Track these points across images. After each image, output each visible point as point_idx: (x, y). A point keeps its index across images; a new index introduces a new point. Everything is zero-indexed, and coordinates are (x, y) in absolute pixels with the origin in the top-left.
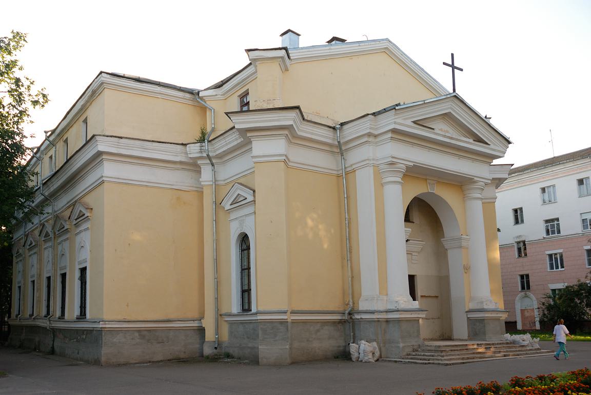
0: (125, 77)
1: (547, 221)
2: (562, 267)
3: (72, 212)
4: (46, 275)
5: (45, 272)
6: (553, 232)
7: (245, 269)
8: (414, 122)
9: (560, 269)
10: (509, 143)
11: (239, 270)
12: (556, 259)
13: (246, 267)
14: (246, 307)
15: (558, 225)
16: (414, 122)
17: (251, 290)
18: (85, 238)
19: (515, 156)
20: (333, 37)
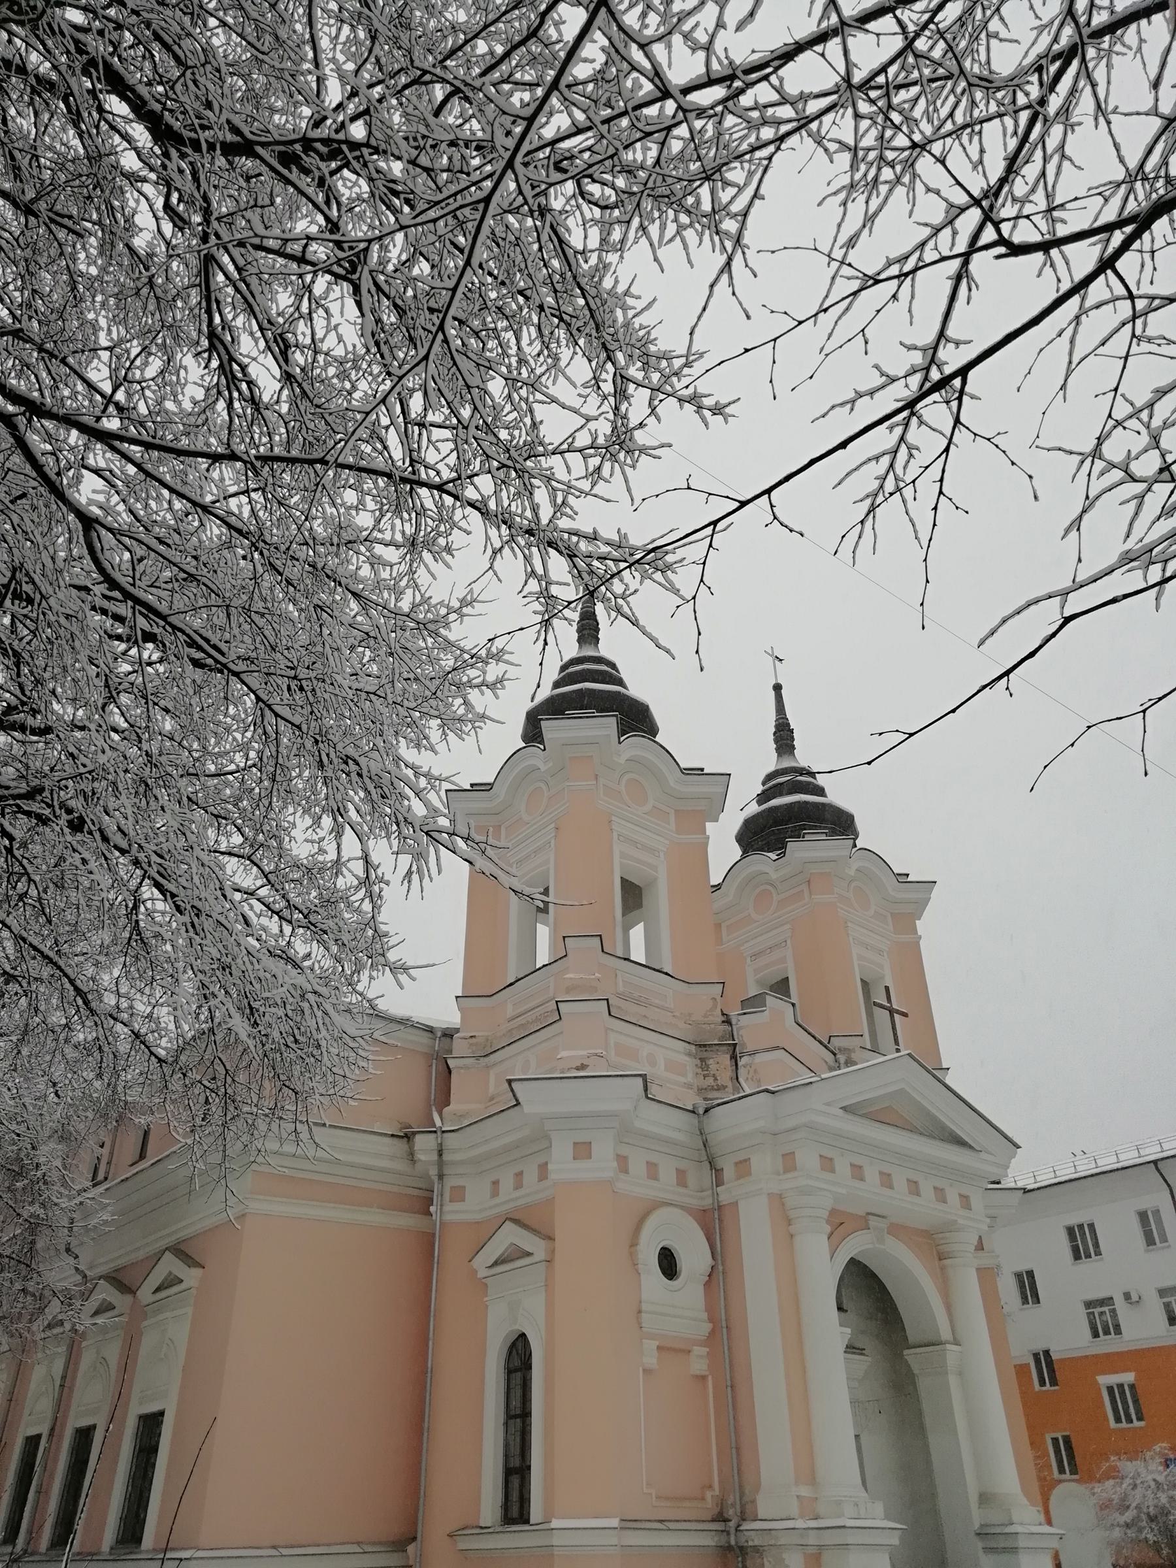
0: (1118, 150)
1: (1089, 1304)
2: (1140, 1419)
3: (827, 296)
4: (76, 1420)
5: (72, 1413)
6: (1107, 1332)
7: (516, 1370)
8: (844, 1108)
9: (1136, 1424)
10: (1019, 1147)
11: (502, 1420)
12: (1122, 1393)
13: (518, 1412)
14: (515, 1512)
15: (1113, 1311)
16: (844, 1108)
17: (529, 1468)
18: (172, 1331)
19: (1022, 1172)
20: (528, 713)
